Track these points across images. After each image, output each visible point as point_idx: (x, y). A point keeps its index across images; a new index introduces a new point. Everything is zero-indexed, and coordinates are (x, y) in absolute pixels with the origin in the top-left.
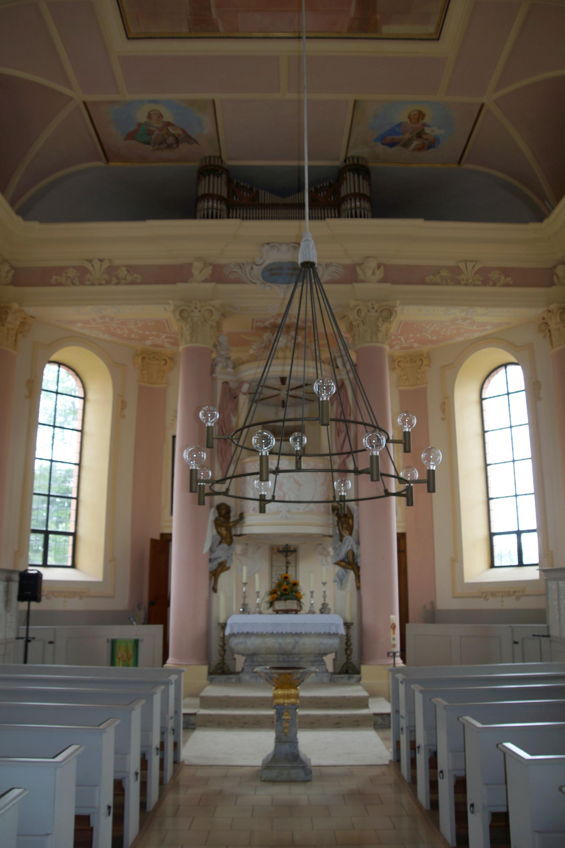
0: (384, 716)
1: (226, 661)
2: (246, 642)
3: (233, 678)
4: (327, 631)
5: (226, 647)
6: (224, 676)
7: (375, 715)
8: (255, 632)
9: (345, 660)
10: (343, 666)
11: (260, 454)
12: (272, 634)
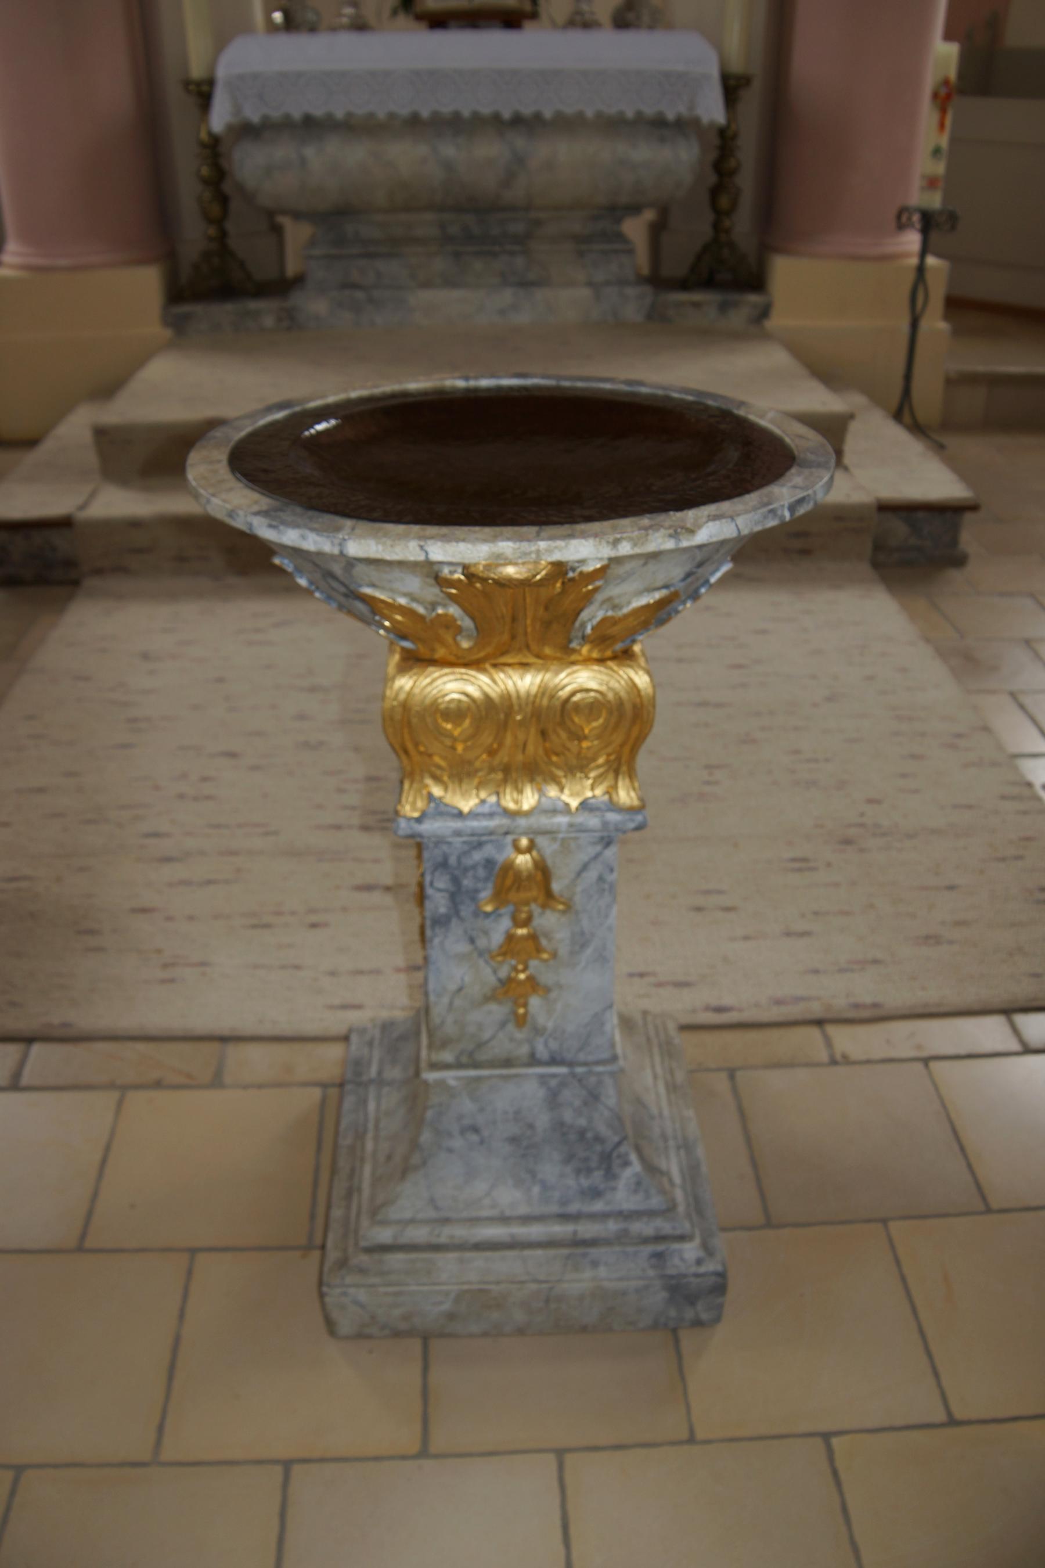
0: (920, 515)
1: (233, 243)
2: (303, 162)
3: (266, 310)
4: (649, 111)
5: (227, 187)
6: (229, 307)
7: (886, 508)
8: (339, 114)
9: (703, 229)
10: (699, 258)
11: (490, 581)
12: (414, 124)
